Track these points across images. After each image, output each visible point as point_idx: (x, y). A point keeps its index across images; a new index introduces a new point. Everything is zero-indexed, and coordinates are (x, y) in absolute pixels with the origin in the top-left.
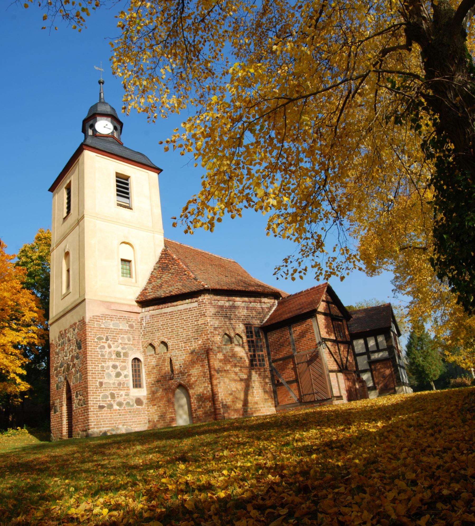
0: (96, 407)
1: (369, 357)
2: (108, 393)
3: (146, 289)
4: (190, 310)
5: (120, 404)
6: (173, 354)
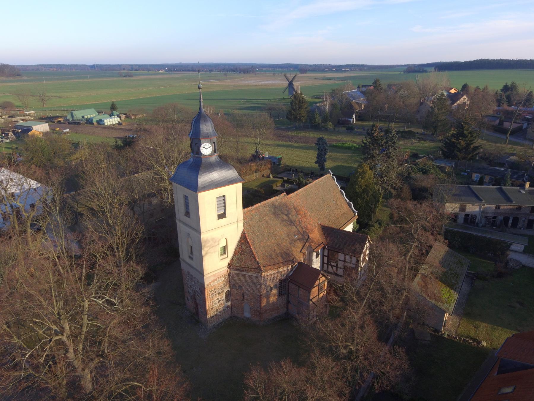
3: (232, 259)
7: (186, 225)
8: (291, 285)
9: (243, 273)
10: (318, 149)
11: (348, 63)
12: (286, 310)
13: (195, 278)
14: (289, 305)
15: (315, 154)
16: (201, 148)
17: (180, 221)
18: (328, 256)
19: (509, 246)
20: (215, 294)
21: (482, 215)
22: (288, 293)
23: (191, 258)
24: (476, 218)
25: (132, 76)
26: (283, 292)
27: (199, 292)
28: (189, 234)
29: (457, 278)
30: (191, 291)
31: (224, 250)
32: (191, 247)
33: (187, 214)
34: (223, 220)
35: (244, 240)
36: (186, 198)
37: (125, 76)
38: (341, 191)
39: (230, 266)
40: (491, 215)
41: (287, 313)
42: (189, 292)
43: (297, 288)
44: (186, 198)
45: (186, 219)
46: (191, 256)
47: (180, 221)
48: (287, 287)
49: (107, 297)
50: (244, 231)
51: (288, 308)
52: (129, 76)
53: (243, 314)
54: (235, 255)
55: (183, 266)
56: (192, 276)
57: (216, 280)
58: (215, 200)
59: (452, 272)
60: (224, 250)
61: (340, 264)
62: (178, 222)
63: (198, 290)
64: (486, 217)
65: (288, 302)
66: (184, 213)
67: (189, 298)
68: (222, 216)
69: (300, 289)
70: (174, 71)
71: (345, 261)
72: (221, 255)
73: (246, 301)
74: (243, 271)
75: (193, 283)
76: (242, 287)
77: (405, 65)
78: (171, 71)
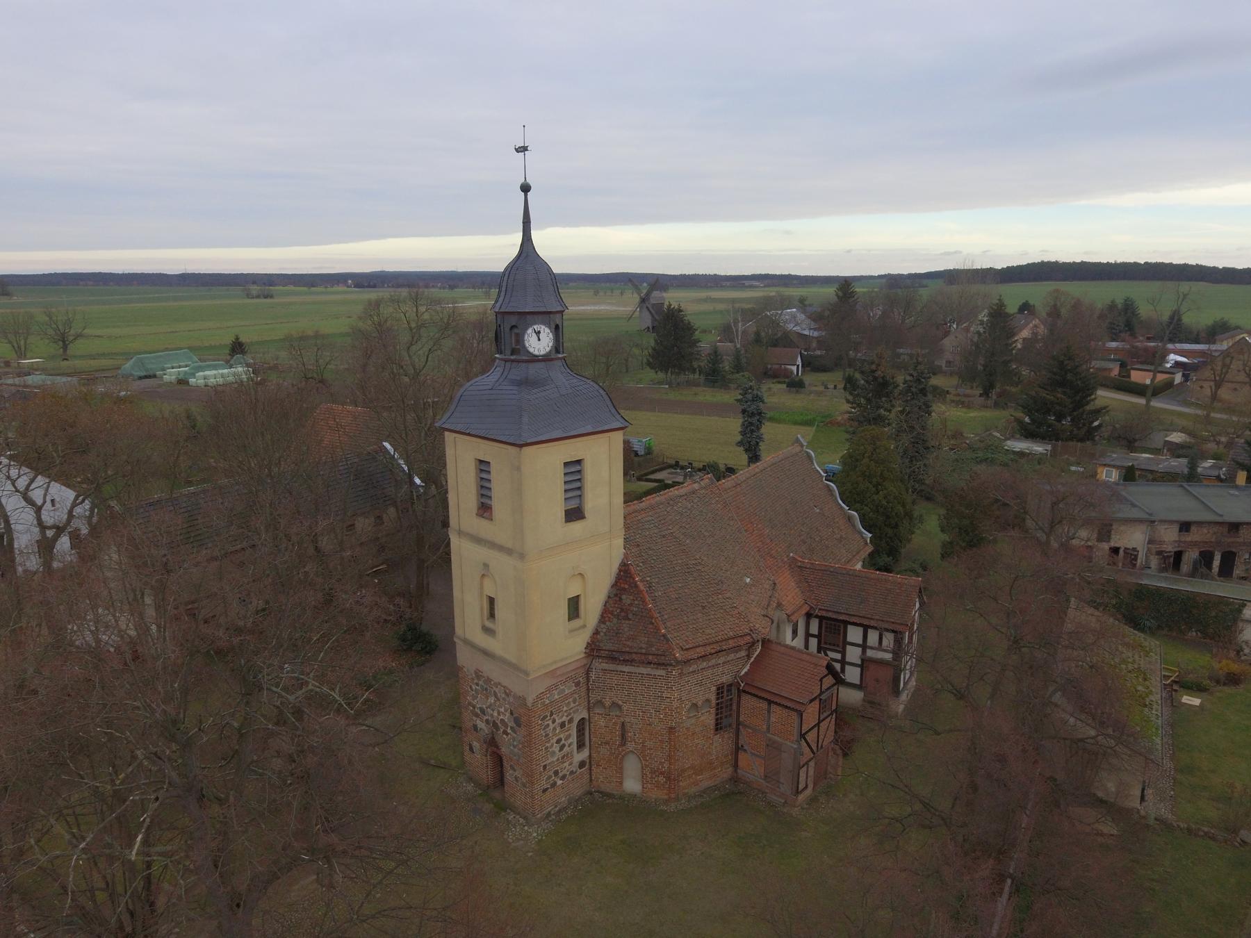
0: (540, 793)
1: (864, 652)
2: (551, 773)
3: (596, 632)
4: (655, 677)
5: (563, 778)
6: (627, 720)
7: (478, 540)
8: (747, 701)
9: (626, 669)
10: (744, 411)
11: (758, 272)
12: (731, 770)
13: (497, 684)
14: (741, 756)
15: (734, 425)
16: (530, 331)
17: (460, 533)
18: (819, 637)
19: (1240, 611)
20: (552, 726)
21: (1149, 549)
22: (738, 723)
23: (488, 631)
24: (1136, 556)
25: (272, 297)
26: (725, 722)
27: (511, 724)
28: (486, 566)
29: (1145, 680)
30: (481, 725)
31: (574, 607)
32: (492, 601)
33: (485, 509)
34: (577, 526)
35: (624, 580)
36: (483, 466)
37: (258, 297)
38: (828, 486)
39: (592, 650)
40: (1170, 548)
41: (735, 780)
42: (475, 727)
43: (764, 705)
44: (483, 466)
45: (482, 527)
46: (488, 624)
47: (460, 533)
48: (734, 707)
49: (313, 685)
50: (626, 556)
51: (736, 766)
52: (266, 297)
53: (621, 783)
54: (602, 619)
55: (464, 658)
56: (488, 680)
57: (556, 686)
58: (561, 470)
59: (1130, 667)
60: (574, 607)
61: (853, 654)
62: (455, 541)
63: (507, 717)
64: (1159, 553)
65: (738, 748)
66: (475, 511)
67: (476, 744)
68: (575, 514)
69: (773, 707)
70: (369, 286)
71: (864, 646)
72: (570, 619)
73: (630, 746)
74: (626, 662)
75: (492, 700)
76: (620, 707)
77: (880, 277)
78: (363, 287)
